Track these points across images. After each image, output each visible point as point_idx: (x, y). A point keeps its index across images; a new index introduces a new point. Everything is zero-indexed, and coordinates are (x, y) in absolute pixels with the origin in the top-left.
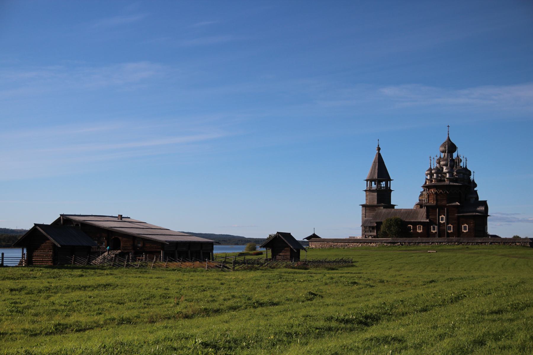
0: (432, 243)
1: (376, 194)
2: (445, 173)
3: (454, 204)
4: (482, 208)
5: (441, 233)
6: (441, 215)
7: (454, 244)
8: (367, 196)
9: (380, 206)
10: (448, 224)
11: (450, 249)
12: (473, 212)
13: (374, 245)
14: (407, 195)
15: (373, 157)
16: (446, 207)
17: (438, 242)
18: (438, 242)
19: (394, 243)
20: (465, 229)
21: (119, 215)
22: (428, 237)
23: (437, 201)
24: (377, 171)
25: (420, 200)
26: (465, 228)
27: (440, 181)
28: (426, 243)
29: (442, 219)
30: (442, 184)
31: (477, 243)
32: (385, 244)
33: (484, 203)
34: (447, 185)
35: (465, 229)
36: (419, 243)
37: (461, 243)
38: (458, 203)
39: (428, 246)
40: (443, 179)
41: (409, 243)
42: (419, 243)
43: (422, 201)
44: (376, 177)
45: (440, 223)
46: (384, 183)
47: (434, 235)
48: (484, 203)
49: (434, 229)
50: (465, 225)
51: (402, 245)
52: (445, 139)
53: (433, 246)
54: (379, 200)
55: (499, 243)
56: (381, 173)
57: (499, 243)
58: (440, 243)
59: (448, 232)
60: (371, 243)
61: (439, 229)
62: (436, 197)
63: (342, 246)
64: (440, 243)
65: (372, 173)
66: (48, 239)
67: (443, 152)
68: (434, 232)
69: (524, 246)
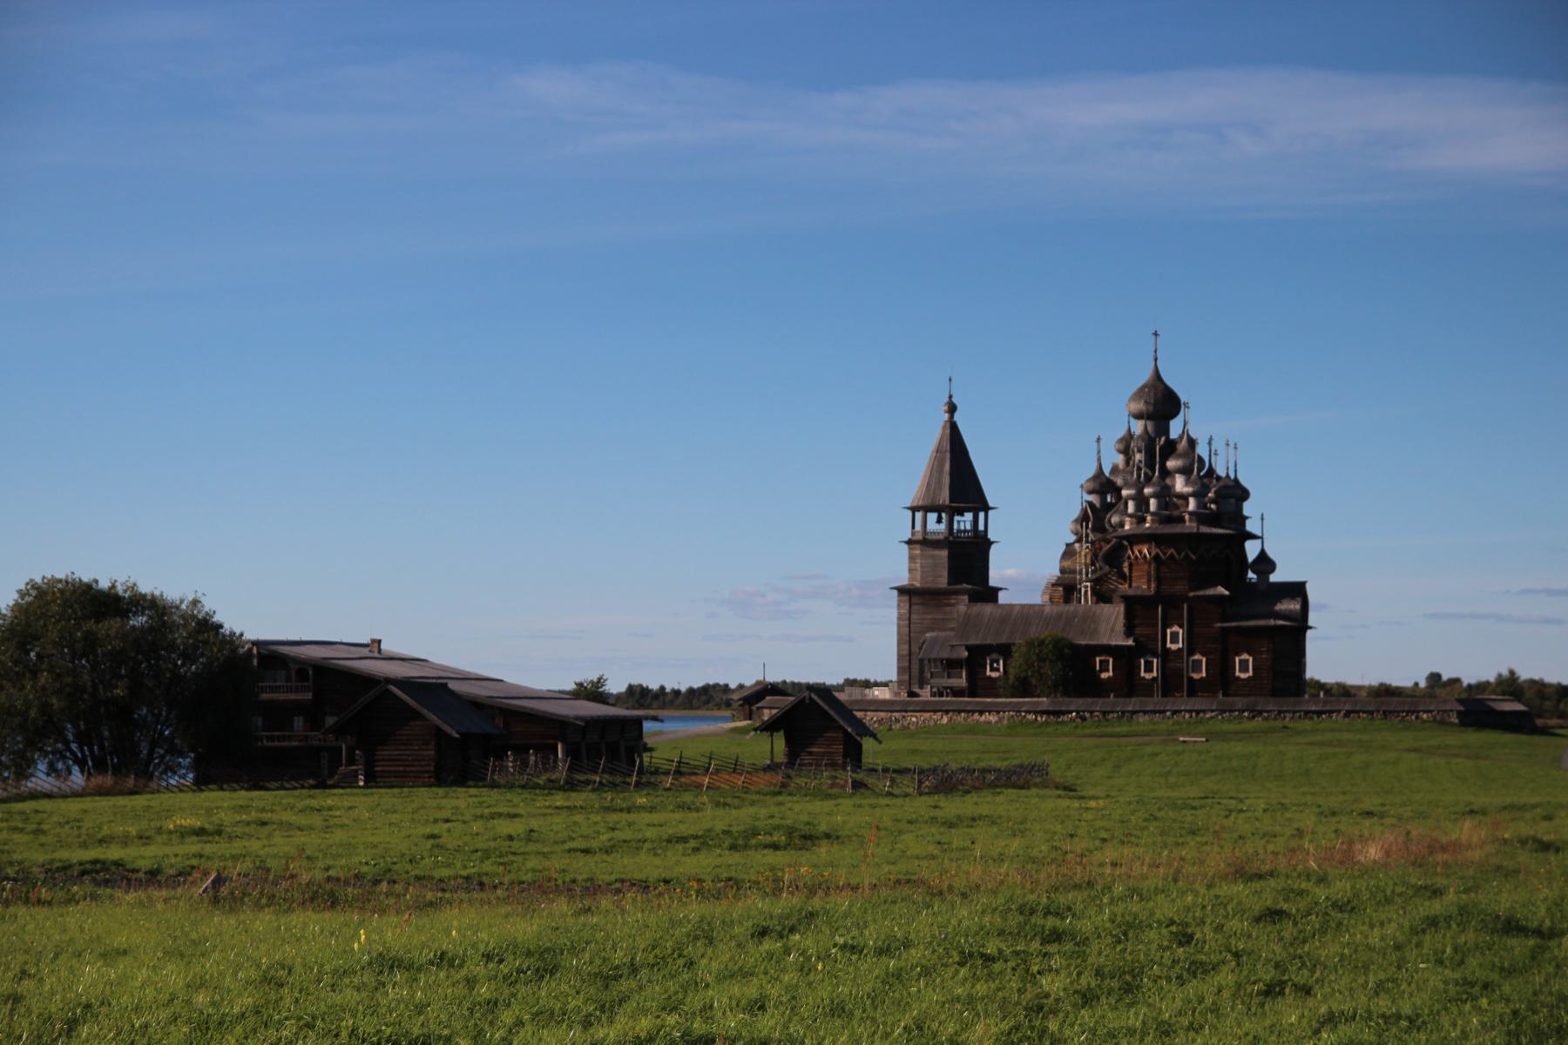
0: (1175, 712)
1: (944, 553)
2: (1184, 497)
3: (1210, 592)
4: (1294, 606)
5: (1172, 683)
6: (1170, 626)
7: (1240, 717)
8: (912, 558)
9: (957, 593)
10: (1191, 652)
11: (1243, 732)
12: (1268, 617)
13: (993, 718)
14: (1029, 554)
15: (932, 435)
16: (1188, 599)
17: (1190, 711)
18: (1190, 711)
19: (1058, 713)
20: (1244, 668)
21: (374, 641)
22: (1130, 695)
23: (1159, 581)
24: (946, 480)
25: (1063, 571)
26: (1244, 664)
27: (1169, 520)
28: (1154, 712)
29: (1174, 638)
30: (1176, 529)
31: (1307, 713)
32: (1031, 717)
33: (1297, 590)
34: (1190, 535)
35: (1244, 668)
36: (1134, 712)
37: (1260, 713)
38: (1221, 590)
39: (1163, 724)
40: (1176, 513)
41: (1105, 713)
42: (1134, 712)
43: (1074, 572)
44: (944, 497)
45: (1166, 651)
46: (969, 516)
47: (1147, 688)
48: (1297, 590)
49: (1149, 669)
50: (1245, 656)
51: (1084, 719)
52: (1145, 376)
53: (1178, 723)
54: (956, 574)
55: (1371, 713)
56: (959, 484)
57: (1371, 713)
58: (1198, 712)
59: (1191, 679)
60: (981, 713)
61: (1163, 668)
62: (1157, 569)
63: (880, 721)
64: (1198, 712)
65: (931, 484)
66: (420, 716)
67: (1138, 416)
68: (1148, 676)
69: (1443, 723)
